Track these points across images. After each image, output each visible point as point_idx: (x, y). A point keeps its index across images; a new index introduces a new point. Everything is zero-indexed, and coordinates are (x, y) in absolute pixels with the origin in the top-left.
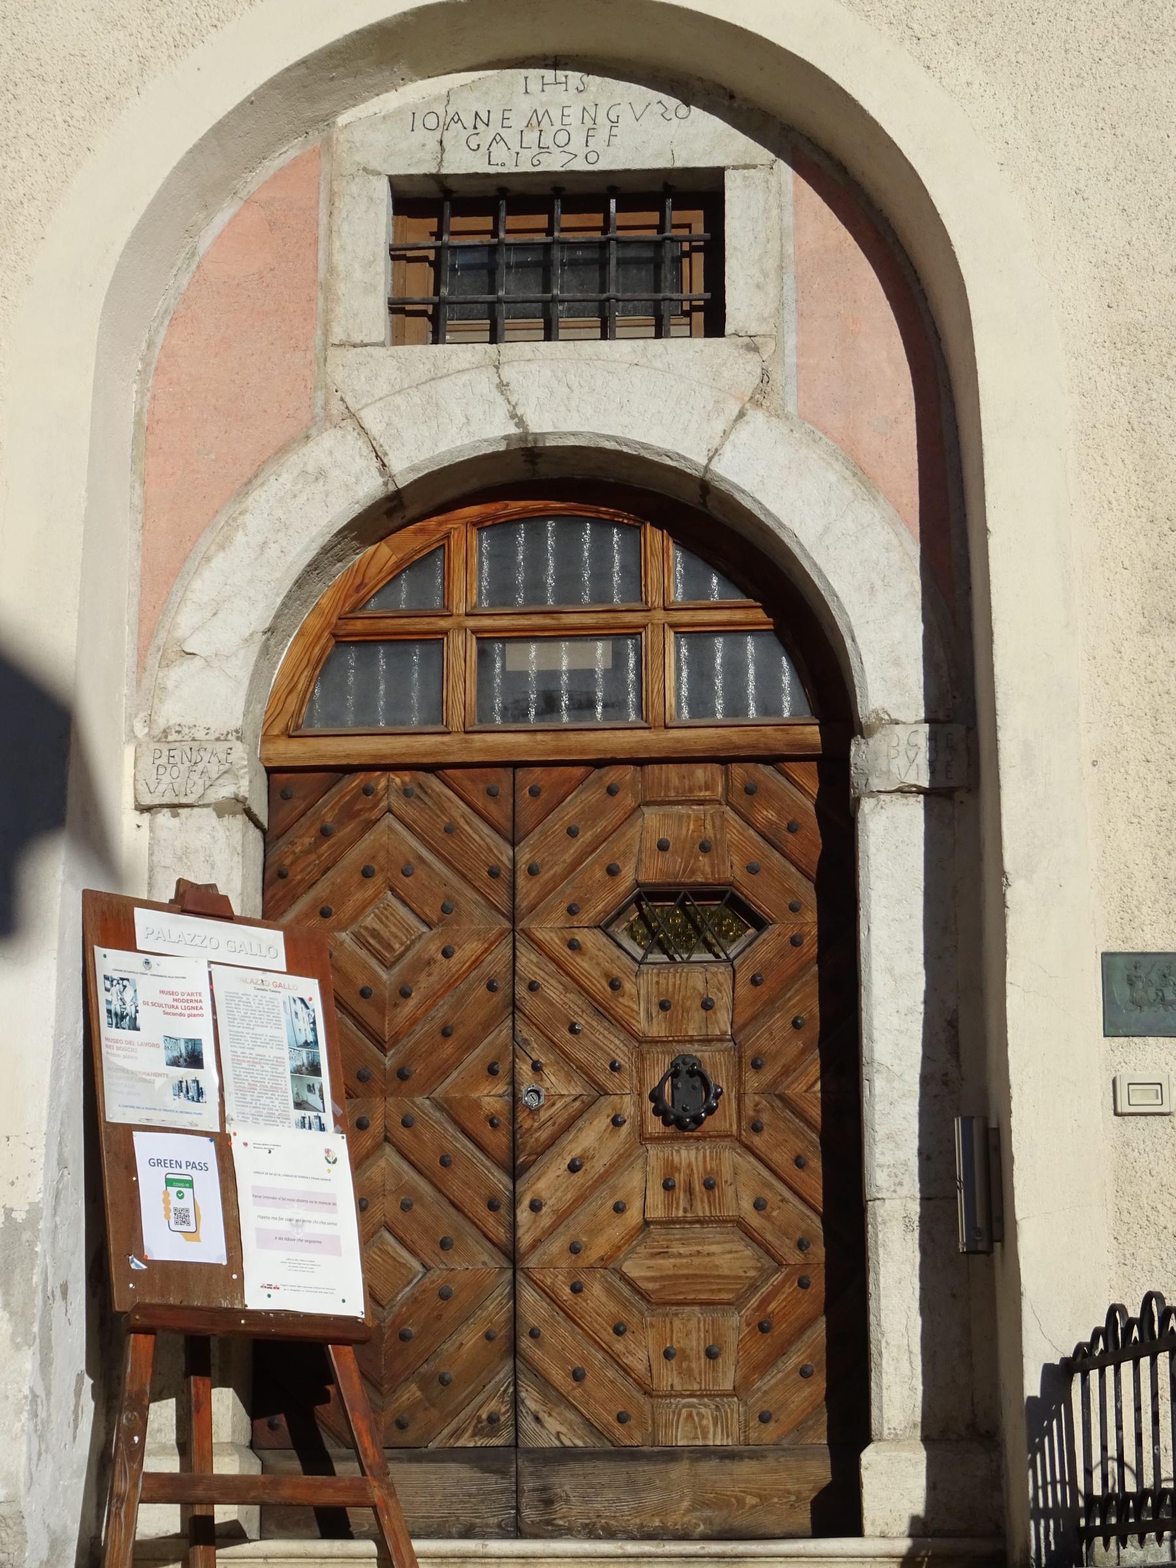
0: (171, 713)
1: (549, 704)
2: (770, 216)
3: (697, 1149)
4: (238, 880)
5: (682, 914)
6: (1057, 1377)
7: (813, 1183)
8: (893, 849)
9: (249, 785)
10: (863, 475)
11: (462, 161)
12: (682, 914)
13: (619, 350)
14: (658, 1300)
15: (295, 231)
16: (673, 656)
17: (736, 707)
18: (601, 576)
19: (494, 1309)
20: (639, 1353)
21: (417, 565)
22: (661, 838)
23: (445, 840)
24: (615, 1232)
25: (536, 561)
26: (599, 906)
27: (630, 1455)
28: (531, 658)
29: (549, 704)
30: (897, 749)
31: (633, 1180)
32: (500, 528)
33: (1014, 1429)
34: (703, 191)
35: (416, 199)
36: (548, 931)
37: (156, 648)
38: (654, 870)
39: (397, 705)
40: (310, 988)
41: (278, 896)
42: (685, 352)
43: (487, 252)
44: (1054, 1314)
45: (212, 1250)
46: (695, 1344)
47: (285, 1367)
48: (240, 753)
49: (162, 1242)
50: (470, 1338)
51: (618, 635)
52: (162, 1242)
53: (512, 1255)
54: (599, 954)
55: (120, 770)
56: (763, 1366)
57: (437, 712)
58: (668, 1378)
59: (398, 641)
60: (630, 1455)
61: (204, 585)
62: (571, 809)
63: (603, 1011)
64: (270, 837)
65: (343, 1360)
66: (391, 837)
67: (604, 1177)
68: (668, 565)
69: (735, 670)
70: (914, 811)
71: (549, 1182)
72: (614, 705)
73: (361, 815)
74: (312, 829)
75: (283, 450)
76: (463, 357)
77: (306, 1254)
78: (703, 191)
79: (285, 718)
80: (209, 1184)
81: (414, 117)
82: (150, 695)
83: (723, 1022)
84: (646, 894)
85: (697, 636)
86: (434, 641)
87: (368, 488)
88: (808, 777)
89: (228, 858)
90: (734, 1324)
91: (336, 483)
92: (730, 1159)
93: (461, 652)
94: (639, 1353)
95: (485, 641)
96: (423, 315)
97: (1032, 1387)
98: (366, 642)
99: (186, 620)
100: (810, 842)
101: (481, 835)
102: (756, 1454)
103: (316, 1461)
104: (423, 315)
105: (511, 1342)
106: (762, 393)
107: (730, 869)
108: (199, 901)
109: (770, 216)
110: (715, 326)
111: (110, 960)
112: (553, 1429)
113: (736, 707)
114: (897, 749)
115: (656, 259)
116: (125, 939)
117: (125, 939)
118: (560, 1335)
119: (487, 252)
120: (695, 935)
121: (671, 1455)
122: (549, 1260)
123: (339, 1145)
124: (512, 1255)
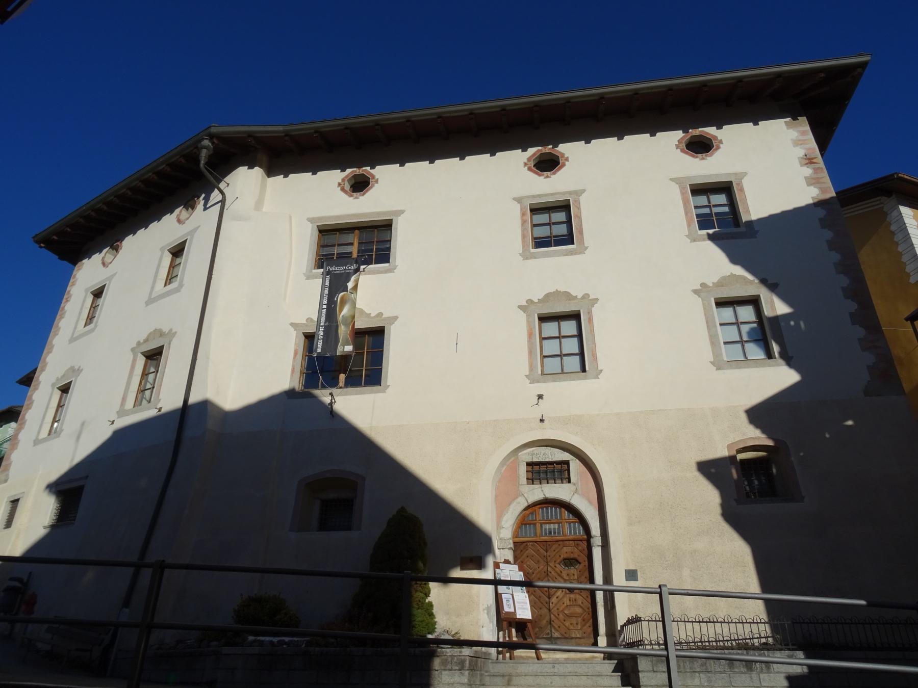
0: (502, 536)
1: (550, 533)
2: (576, 466)
3: (417, 591)
4: (511, 559)
5: (570, 562)
6: (622, 627)
7: (589, 600)
8: (597, 553)
9: (512, 545)
10: (590, 502)
11: (535, 460)
12: (570, 562)
13: (557, 485)
14: (569, 616)
15: (514, 469)
16: (567, 526)
17: (575, 533)
18: (556, 515)
19: (548, 618)
20: (567, 624)
21: (532, 513)
22: (567, 551)
23: (537, 551)
24: (563, 606)
25: (547, 513)
26: (558, 561)
27: (567, 638)
28: (547, 526)
29: (550, 533)
30: (597, 541)
31: (565, 599)
32: (542, 508)
33: (617, 634)
34: (567, 463)
35: (528, 464)
36: (552, 564)
37: (499, 527)
38: (566, 556)
39: (526, 533)
40: (521, 573)
41: (516, 559)
42: (566, 485)
43: (540, 472)
44: (621, 620)
45: (512, 610)
46: (574, 622)
47: (521, 626)
48: (511, 541)
49: (506, 609)
50: (544, 622)
51: (559, 523)
52: (506, 609)
53: (550, 610)
54: (559, 568)
55: (496, 544)
56: (584, 626)
57: (536, 535)
58: (571, 627)
59: (530, 524)
60: (567, 638)
61: (505, 518)
62: (554, 547)
63: (560, 576)
64: (514, 551)
65: (529, 625)
66: (530, 551)
67: (560, 600)
68: (566, 514)
69: (575, 528)
70: (599, 549)
71: (554, 600)
72: (559, 533)
73: (526, 548)
74: (519, 549)
75: (514, 500)
76: (536, 486)
77: (524, 612)
78: (567, 463)
79: (516, 535)
80: (511, 601)
81: (529, 453)
82: (499, 533)
83: (576, 577)
84: (565, 559)
85: (570, 523)
86: (535, 524)
87: (526, 505)
88: (585, 543)
89: (510, 556)
90: (580, 620)
91: (519, 505)
92: (578, 596)
93: (538, 525)
94: (567, 624)
95: (541, 524)
96: (531, 480)
97: (619, 628)
98: (526, 524)
99: (503, 523)
100: (586, 551)
101: (542, 551)
102: (583, 638)
103: (525, 639)
104: (531, 480)
105: (550, 622)
106: (576, 491)
107: (576, 556)
108: (507, 562)
109: (576, 466)
110: (569, 482)
111: (497, 571)
112: (556, 635)
113: (575, 533)
114: (597, 541)
115: (561, 472)
116: (499, 568)
117: (499, 568)
118: (556, 621)
119: (540, 472)
120: (572, 565)
121: (572, 638)
122: (554, 611)
123: (527, 595)
124: (550, 610)
